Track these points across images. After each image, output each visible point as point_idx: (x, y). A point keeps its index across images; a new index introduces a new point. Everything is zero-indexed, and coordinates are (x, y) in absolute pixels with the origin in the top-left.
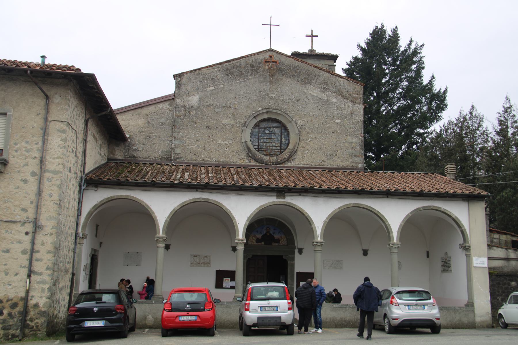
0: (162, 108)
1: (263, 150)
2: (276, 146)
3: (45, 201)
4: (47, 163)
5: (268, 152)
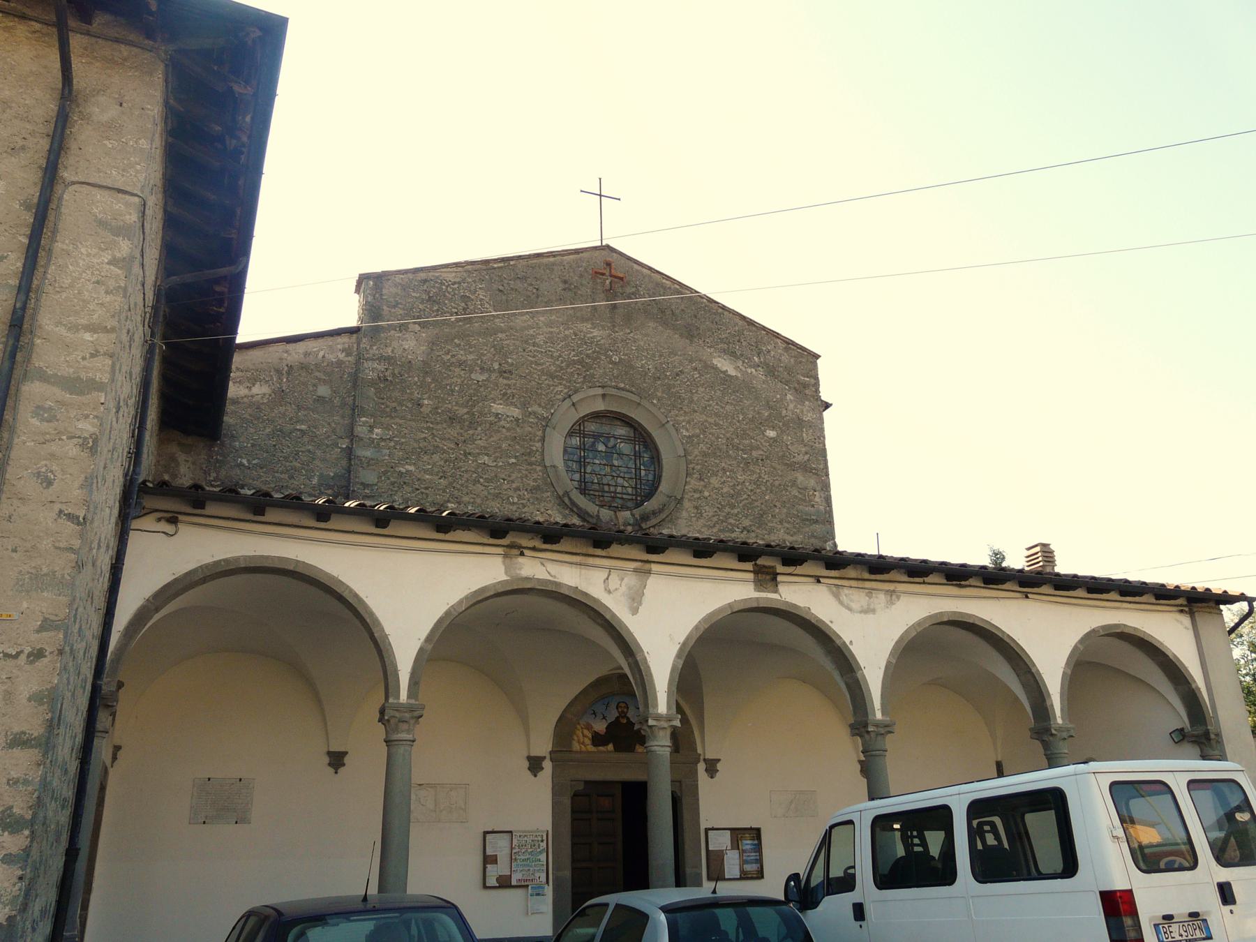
0: (324, 357)
1: (591, 492)
2: (625, 486)
3: (15, 502)
4: (38, 341)
5: (606, 499)
